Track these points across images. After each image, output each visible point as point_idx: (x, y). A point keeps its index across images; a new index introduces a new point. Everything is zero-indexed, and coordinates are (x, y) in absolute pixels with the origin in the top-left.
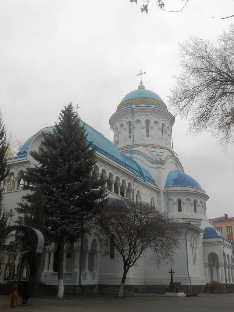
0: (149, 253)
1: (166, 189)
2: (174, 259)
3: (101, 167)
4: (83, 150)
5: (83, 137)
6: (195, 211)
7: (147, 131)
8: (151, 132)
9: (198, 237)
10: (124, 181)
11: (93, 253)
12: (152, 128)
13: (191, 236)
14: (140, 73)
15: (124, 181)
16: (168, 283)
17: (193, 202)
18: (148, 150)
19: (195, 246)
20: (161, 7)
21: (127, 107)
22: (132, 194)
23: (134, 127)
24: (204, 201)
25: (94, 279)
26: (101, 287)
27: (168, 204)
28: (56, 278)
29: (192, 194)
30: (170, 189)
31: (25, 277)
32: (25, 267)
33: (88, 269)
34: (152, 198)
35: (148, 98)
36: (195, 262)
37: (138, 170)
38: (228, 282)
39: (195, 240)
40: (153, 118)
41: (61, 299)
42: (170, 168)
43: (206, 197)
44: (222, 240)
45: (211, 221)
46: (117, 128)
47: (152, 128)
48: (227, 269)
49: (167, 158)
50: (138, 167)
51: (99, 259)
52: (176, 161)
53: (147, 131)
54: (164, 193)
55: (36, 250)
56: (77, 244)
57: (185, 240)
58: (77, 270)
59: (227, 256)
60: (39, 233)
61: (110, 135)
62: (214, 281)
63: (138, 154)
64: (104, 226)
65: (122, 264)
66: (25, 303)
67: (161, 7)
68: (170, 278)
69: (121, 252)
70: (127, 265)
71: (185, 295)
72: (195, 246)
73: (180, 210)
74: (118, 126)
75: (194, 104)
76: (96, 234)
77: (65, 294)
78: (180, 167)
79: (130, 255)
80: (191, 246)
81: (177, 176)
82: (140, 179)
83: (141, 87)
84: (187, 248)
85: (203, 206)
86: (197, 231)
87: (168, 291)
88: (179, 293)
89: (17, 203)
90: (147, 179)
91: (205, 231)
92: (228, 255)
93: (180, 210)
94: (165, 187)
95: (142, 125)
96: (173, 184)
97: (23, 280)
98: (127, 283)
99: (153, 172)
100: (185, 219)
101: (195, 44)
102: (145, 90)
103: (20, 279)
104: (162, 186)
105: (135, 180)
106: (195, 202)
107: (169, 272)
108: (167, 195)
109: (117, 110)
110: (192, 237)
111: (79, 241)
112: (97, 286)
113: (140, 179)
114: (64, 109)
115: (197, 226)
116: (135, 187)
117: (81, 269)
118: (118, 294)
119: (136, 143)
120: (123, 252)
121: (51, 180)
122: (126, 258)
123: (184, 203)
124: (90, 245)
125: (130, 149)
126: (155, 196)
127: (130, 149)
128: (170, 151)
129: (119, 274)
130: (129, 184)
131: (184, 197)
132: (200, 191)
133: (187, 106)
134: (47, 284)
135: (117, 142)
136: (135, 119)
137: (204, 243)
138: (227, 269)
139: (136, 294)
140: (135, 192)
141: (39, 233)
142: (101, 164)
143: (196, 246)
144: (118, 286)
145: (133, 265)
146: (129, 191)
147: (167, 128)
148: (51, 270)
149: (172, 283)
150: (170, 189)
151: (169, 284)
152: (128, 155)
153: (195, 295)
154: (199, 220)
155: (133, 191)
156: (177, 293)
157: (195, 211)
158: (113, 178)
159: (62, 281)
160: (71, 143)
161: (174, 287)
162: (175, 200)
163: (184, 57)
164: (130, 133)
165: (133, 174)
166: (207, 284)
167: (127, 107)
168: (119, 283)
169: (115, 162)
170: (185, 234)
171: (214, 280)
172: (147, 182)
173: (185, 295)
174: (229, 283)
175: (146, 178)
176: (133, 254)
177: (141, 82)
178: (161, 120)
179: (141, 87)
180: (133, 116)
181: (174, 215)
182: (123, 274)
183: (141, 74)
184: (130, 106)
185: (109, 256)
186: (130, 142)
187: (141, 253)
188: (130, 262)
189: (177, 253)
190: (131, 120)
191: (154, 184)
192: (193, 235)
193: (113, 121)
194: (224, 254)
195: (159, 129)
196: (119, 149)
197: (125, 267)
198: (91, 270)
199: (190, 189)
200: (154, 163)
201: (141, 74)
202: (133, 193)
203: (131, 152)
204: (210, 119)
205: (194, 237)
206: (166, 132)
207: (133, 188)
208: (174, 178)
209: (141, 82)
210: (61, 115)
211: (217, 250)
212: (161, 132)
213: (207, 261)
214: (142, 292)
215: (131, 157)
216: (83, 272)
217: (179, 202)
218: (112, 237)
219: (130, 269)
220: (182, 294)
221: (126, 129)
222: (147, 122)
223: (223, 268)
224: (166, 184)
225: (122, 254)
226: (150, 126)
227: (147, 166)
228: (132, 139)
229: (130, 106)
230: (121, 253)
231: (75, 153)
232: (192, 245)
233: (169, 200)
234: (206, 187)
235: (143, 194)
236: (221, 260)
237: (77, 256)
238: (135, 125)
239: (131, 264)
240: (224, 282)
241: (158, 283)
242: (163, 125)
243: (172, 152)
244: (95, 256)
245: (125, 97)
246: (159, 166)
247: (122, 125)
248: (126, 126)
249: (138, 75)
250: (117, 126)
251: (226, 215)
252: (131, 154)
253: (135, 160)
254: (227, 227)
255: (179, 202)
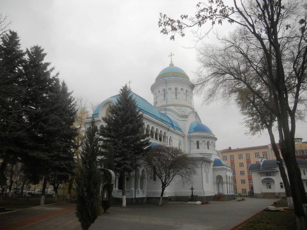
0: (177, 178)
1: (189, 134)
2: (194, 182)
3: (146, 123)
4: (135, 116)
5: (135, 107)
6: (208, 149)
7: (176, 95)
8: (179, 96)
9: (210, 166)
10: (161, 131)
11: (143, 178)
12: (179, 93)
13: (205, 165)
14: (170, 54)
15: (161, 131)
16: (190, 195)
17: (206, 143)
18: (177, 108)
19: (208, 171)
20: (183, 36)
21: (162, 79)
22: (166, 139)
23: (167, 93)
24: (214, 142)
25: (144, 193)
26: (148, 198)
27: (190, 144)
28: (121, 194)
29: (206, 137)
30: (192, 134)
31: (106, 198)
32: (105, 192)
33: (139, 187)
34: (180, 141)
35: (177, 73)
36: (207, 182)
37: (170, 123)
38: (229, 193)
39: (208, 167)
40: (179, 86)
41: (124, 207)
42: (191, 120)
43: (216, 139)
44: (225, 167)
45: (220, 152)
46: (156, 93)
47: (179, 93)
48: (228, 185)
49: (189, 114)
50: (170, 120)
51: (146, 182)
52: (195, 115)
53: (176, 95)
54: (187, 137)
55: (111, 182)
56: (133, 173)
57: (201, 168)
58: (133, 189)
59: (228, 177)
60: (112, 172)
61: (150, 98)
62: (220, 193)
63: (170, 111)
64: (149, 162)
65: (161, 185)
66: (105, 212)
67: (183, 36)
68: (191, 192)
69: (160, 178)
70: (164, 186)
71: (201, 203)
72: (208, 171)
73: (198, 148)
74: (157, 92)
75: (205, 88)
76: (145, 166)
77: (127, 204)
78: (198, 119)
79: (166, 180)
80: (205, 171)
81: (196, 125)
82: (171, 129)
83: (171, 65)
84: (202, 173)
85: (213, 145)
86: (209, 162)
87: (190, 200)
88: (197, 202)
89: (59, 71)
90: (177, 129)
91: (214, 162)
92: (229, 176)
93: (198, 148)
94: (188, 133)
95: (173, 91)
96: (194, 131)
97: (105, 200)
98: (164, 196)
99: (180, 123)
100: (202, 154)
101: (206, 48)
102: (175, 67)
103: (103, 199)
104: (186, 133)
105: (168, 130)
106: (208, 142)
107: (191, 189)
108: (189, 139)
109: (155, 81)
110: (205, 166)
111: (134, 171)
112: (146, 198)
113: (171, 129)
114: (122, 88)
115: (209, 159)
116: (169, 134)
117: (136, 188)
118: (159, 203)
119: (169, 103)
120: (161, 178)
121: (116, 136)
122: (164, 181)
123: (201, 144)
124: (140, 173)
125: (164, 108)
126: (182, 139)
127: (164, 107)
128: (191, 109)
129: (159, 191)
130: (165, 133)
131: (201, 139)
132: (211, 135)
133: (201, 89)
134: (115, 197)
135: (156, 103)
136: (168, 88)
137: (213, 169)
138: (228, 185)
139: (170, 202)
140: (169, 138)
141: (112, 172)
142: (146, 121)
143: (209, 171)
144: (159, 198)
145: (167, 186)
146: (164, 137)
147: (189, 92)
148: (117, 189)
149: (192, 195)
150: (192, 134)
151: (191, 196)
152: (163, 112)
153: (207, 203)
154: (211, 155)
155: (167, 137)
156: (195, 202)
157: (208, 149)
158: (154, 130)
159: (125, 196)
160: (127, 111)
161: (193, 198)
162: (195, 141)
163: (199, 56)
164: (165, 96)
165: (167, 126)
166: (216, 195)
167: (162, 79)
168: (160, 196)
169: (156, 119)
170: (201, 165)
171: (220, 192)
172: (176, 130)
173: (201, 203)
174: (230, 194)
175: (175, 128)
176: (168, 179)
177: (171, 60)
178: (185, 87)
179: (171, 65)
180: (166, 85)
181: (193, 152)
182: (161, 190)
183: (171, 55)
184: (165, 79)
185: (153, 179)
186: (164, 103)
187: (173, 178)
188: (166, 184)
189: (195, 178)
190: (165, 88)
191: (181, 131)
192: (206, 164)
193: (153, 88)
194: (227, 176)
195: (184, 94)
196: (158, 108)
197: (163, 187)
198: (142, 188)
199: (205, 134)
200: (181, 117)
201: (171, 55)
202: (167, 138)
203: (166, 110)
204: (215, 96)
205: (207, 166)
206: (188, 95)
207: (167, 135)
208: (195, 126)
209: (171, 60)
210: (120, 93)
211: (222, 173)
212: (185, 96)
213: (215, 181)
214: (174, 201)
215: (166, 113)
216: (137, 189)
217: (198, 143)
218: (154, 168)
219: (166, 188)
220: (199, 202)
221: (162, 94)
222: (176, 89)
223: (226, 185)
224: (189, 131)
225: (161, 179)
226: (178, 92)
227: (176, 119)
228: (166, 101)
229: (165, 79)
230: (160, 179)
231: (130, 118)
232: (206, 171)
233: (191, 141)
234: (215, 132)
235: (174, 138)
236: (224, 180)
237: (133, 180)
238: (168, 91)
239: (167, 185)
240: (226, 194)
241: (184, 195)
242: (187, 91)
243: (193, 109)
244: (144, 180)
245: (161, 72)
246: (184, 119)
247: (159, 91)
248: (162, 92)
249: (173, 55)
250: (156, 92)
251: (230, 147)
252: (165, 111)
253: (167, 115)
254: (230, 156)
255: (198, 143)
